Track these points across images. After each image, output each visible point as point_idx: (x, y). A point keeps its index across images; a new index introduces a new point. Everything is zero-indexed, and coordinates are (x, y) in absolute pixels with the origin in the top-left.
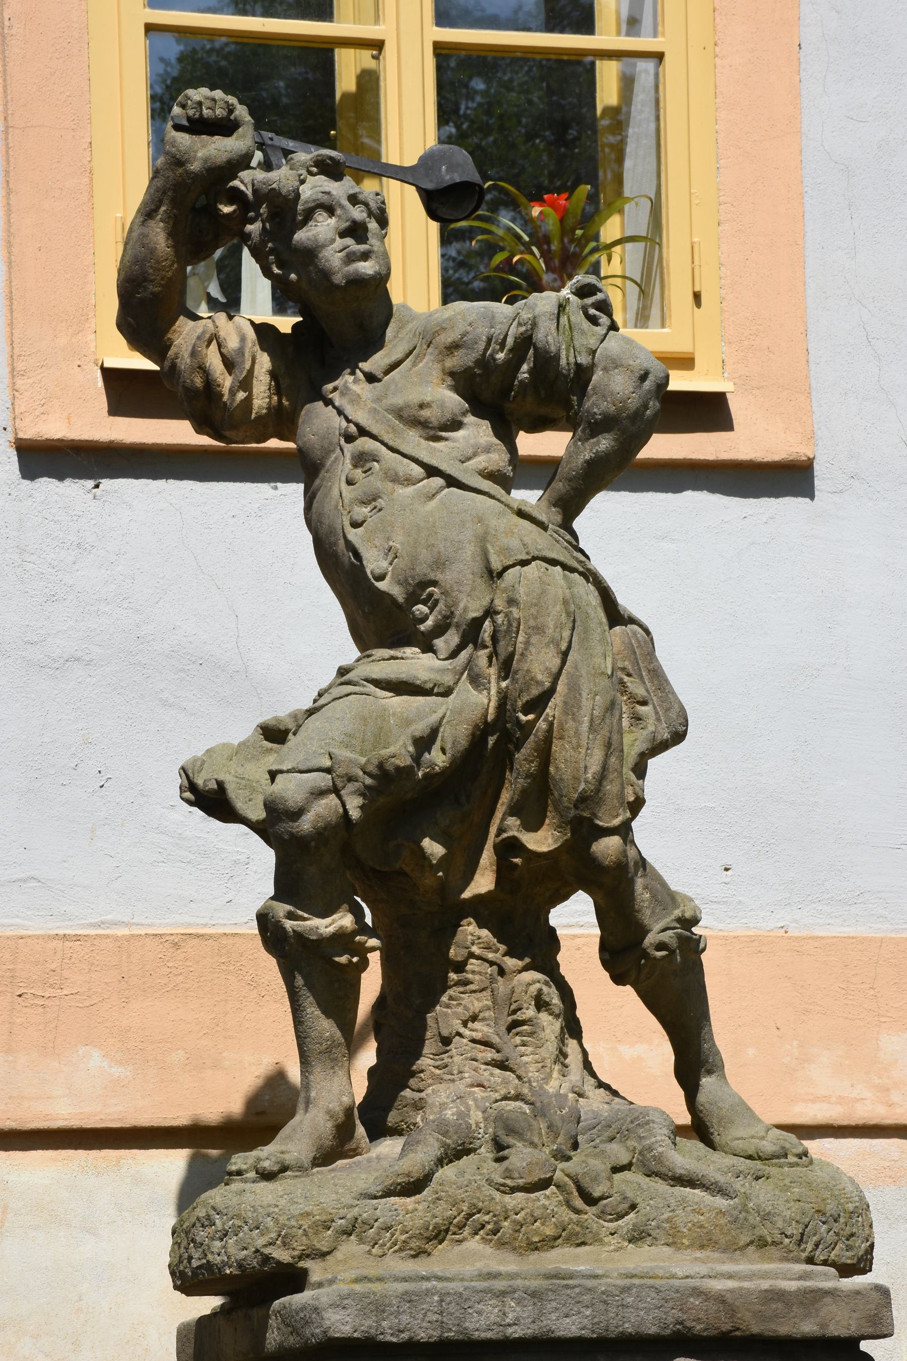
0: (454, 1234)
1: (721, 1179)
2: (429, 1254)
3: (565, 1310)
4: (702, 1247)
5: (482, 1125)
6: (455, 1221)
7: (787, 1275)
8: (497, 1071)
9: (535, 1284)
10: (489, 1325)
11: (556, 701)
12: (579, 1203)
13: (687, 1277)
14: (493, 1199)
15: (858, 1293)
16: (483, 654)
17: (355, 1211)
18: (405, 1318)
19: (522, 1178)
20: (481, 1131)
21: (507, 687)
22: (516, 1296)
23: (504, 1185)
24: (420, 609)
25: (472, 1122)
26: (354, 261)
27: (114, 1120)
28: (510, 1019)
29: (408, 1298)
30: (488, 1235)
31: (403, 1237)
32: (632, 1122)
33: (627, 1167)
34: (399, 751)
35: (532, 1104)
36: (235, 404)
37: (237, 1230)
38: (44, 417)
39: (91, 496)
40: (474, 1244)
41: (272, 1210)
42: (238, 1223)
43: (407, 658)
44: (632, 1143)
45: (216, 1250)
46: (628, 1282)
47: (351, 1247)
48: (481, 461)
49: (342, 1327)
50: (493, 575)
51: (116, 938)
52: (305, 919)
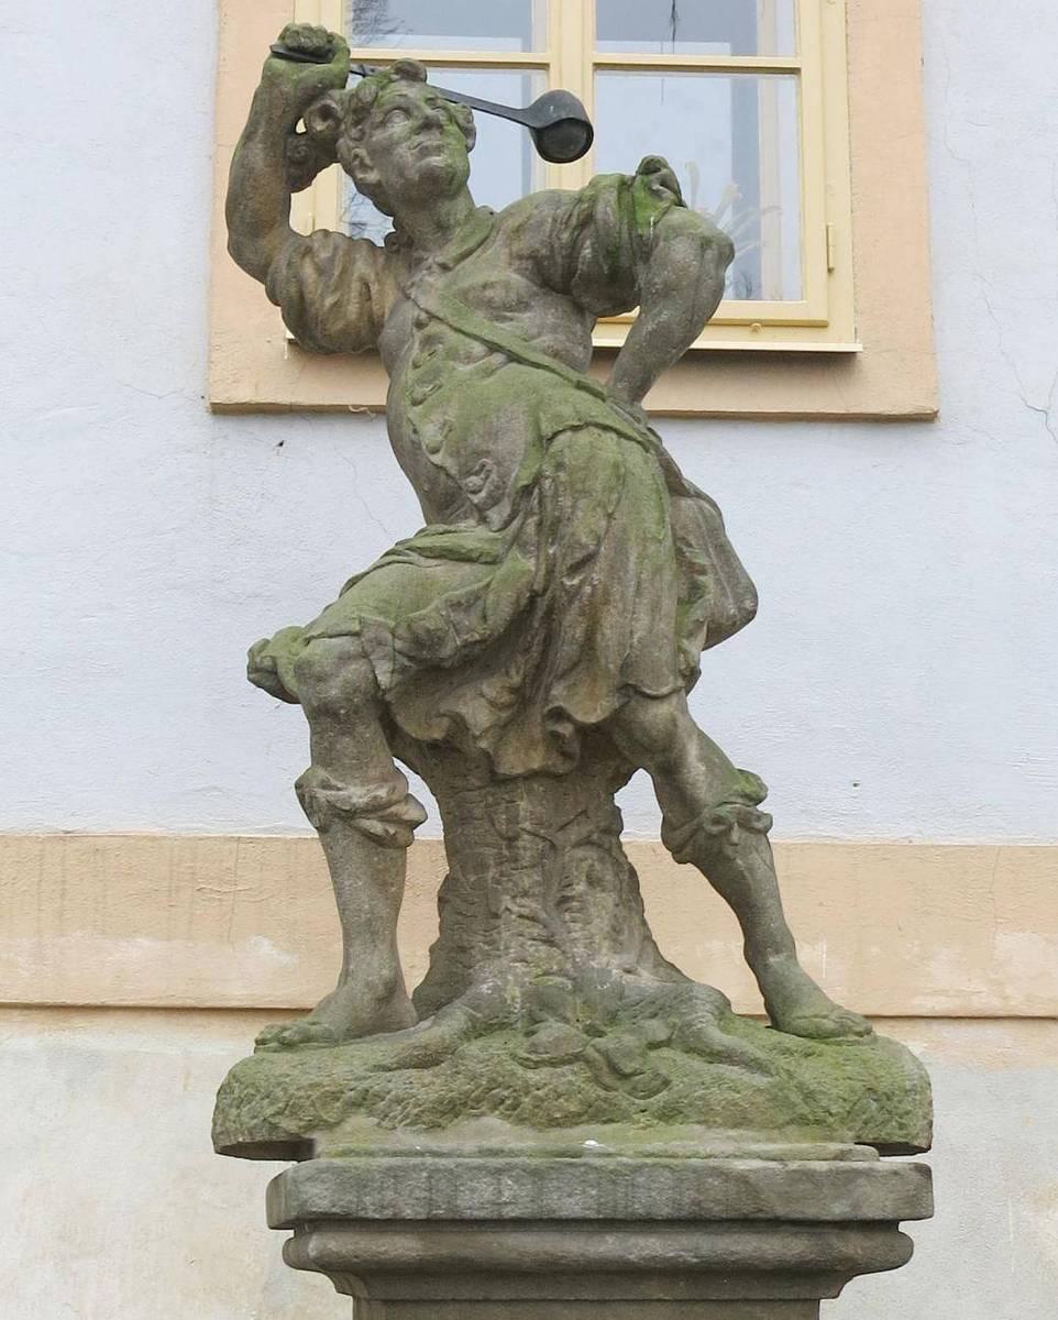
0: (472, 1108)
1: (760, 1054)
2: (444, 1128)
3: (568, 1189)
4: (735, 1126)
5: (519, 1000)
6: (473, 1095)
7: (812, 1153)
8: (543, 948)
9: (535, 1162)
10: (482, 1203)
11: (601, 564)
12: (608, 1079)
13: (710, 1156)
14: (515, 1074)
15: (896, 1173)
16: (532, 520)
17: (365, 1084)
18: (390, 1195)
19: (547, 1053)
20: (518, 1006)
21: (554, 554)
22: (514, 1174)
23: (527, 1059)
24: (474, 480)
25: (507, 996)
26: (426, 155)
27: (282, 1002)
28: (559, 895)
29: (394, 1174)
30: (507, 1110)
31: (416, 1111)
32: (675, 998)
33: (667, 1043)
34: (431, 616)
35: (574, 979)
36: (325, 309)
37: (250, 1099)
38: (235, 384)
39: (275, 452)
40: (493, 1121)
41: (282, 1079)
42: (253, 1092)
43: (461, 531)
44: (674, 1019)
45: (232, 1118)
46: (640, 1161)
47: (360, 1121)
48: (547, 340)
49: (319, 1201)
50: (544, 442)
51: (286, 841)
52: (339, 789)
